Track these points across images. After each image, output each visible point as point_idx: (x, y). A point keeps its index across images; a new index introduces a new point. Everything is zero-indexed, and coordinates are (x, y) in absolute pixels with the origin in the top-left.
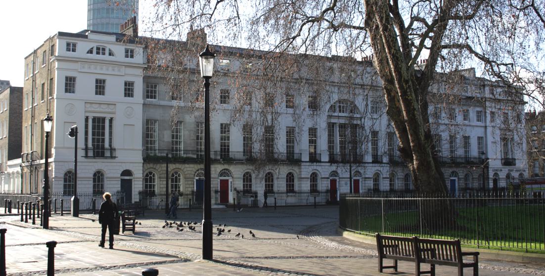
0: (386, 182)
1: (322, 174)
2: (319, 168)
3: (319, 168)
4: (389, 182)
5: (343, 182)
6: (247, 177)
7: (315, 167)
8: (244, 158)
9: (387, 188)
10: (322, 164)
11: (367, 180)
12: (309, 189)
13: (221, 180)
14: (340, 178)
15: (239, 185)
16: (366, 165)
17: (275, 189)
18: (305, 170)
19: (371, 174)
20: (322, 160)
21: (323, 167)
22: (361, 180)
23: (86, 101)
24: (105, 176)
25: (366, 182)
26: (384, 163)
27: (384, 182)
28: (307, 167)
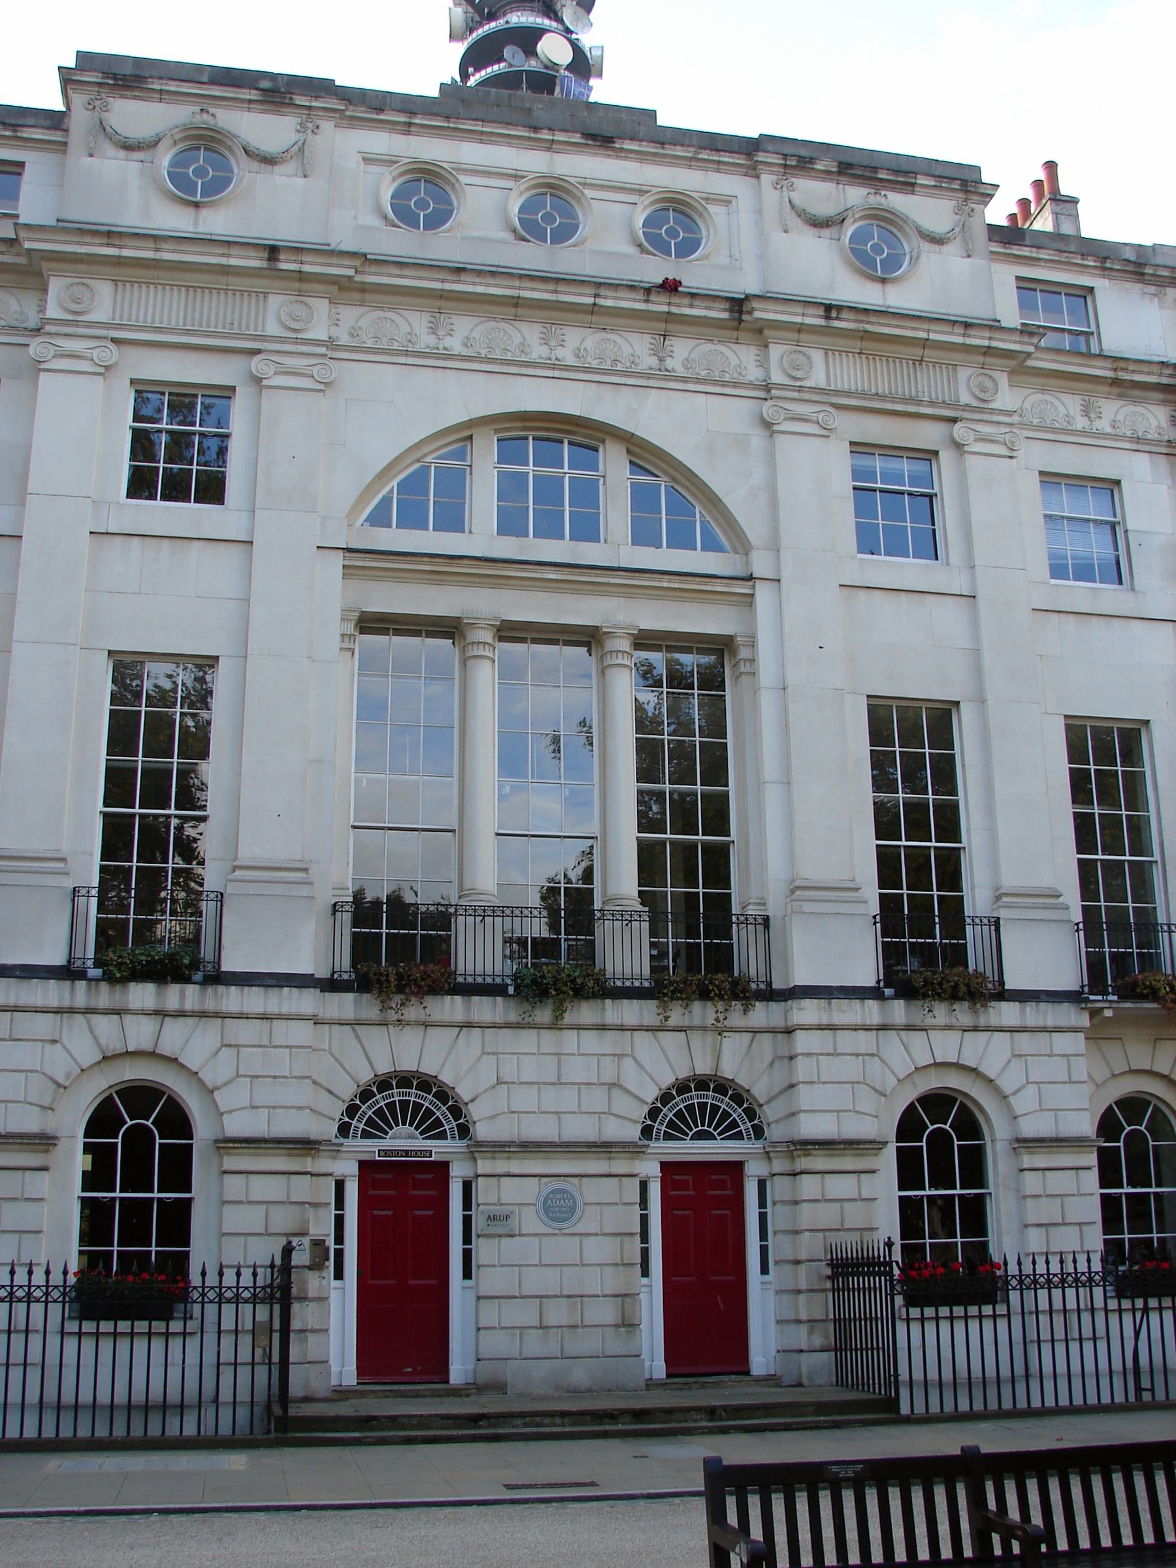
0: (1060, 1182)
1: (1021, 1104)
2: (193, 1044)
3: (193, 1044)
4: (1091, 1180)
5: (512, 1192)
6: (939, 1139)
7: (140, 1033)
8: (511, 967)
9: (1066, 1240)
10: (232, 999)
11: (819, 1162)
12: (1095, 1240)
13: (667, 1168)
14: (478, 1149)
15: (870, 1204)
16: (807, 1012)
17: (1008, 1239)
18: (832, 1068)
19: (867, 1102)
20: (228, 965)
21: (246, 1031)
22: (754, 1170)
23: (1109, 597)
24: (203, 1130)
25: (809, 1186)
26: (470, 990)
27: (1032, 1182)
28: (44, 1025)
